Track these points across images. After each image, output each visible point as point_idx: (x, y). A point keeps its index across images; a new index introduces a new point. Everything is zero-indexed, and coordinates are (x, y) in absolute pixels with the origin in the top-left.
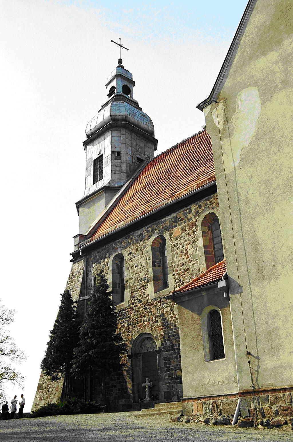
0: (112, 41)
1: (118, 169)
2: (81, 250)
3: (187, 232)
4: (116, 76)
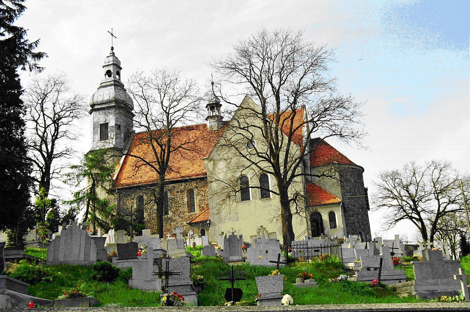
0: (108, 32)
1: (119, 136)
2: (89, 189)
3: (180, 194)
4: (113, 64)
